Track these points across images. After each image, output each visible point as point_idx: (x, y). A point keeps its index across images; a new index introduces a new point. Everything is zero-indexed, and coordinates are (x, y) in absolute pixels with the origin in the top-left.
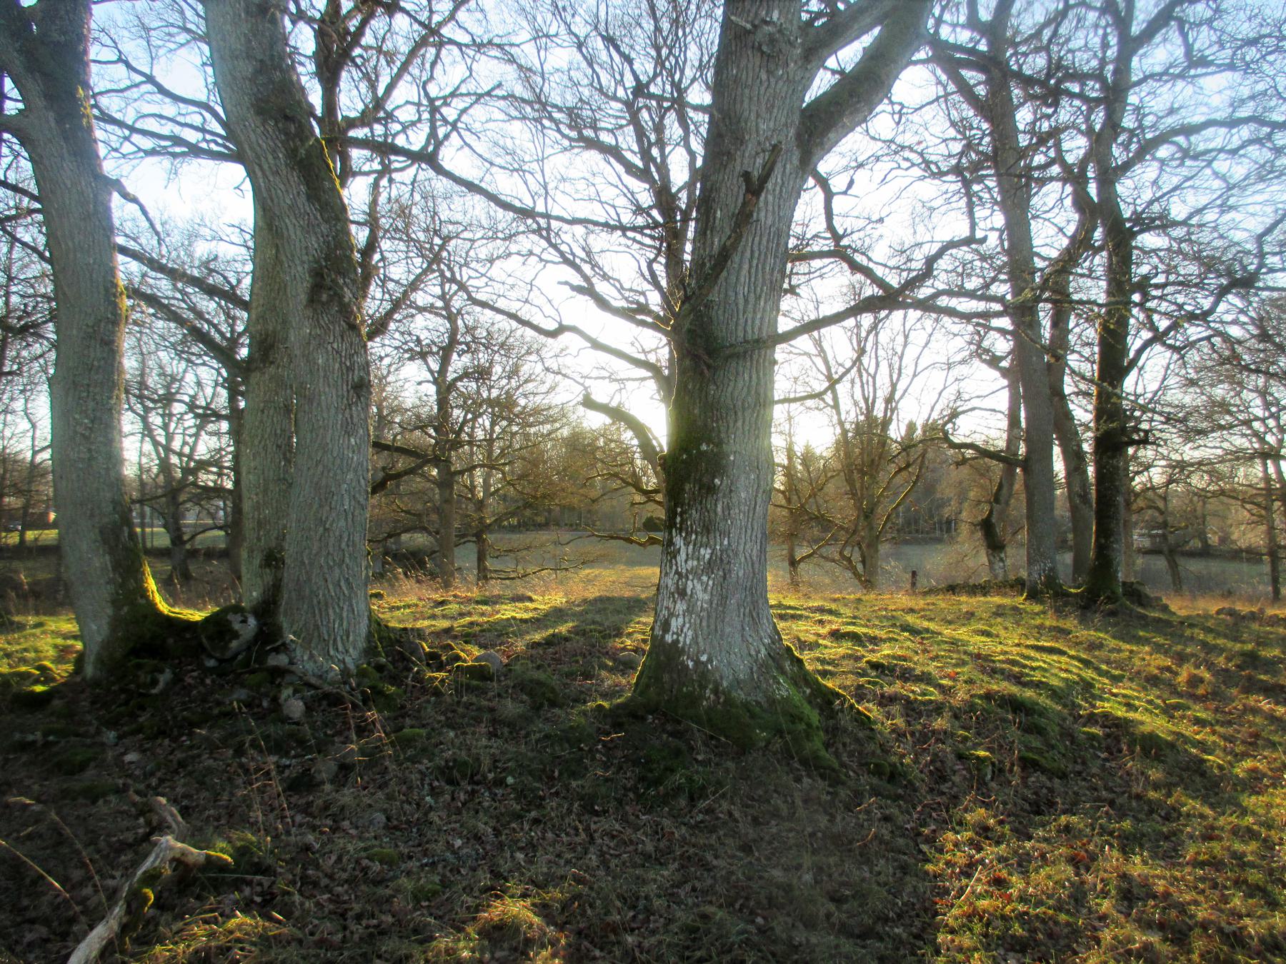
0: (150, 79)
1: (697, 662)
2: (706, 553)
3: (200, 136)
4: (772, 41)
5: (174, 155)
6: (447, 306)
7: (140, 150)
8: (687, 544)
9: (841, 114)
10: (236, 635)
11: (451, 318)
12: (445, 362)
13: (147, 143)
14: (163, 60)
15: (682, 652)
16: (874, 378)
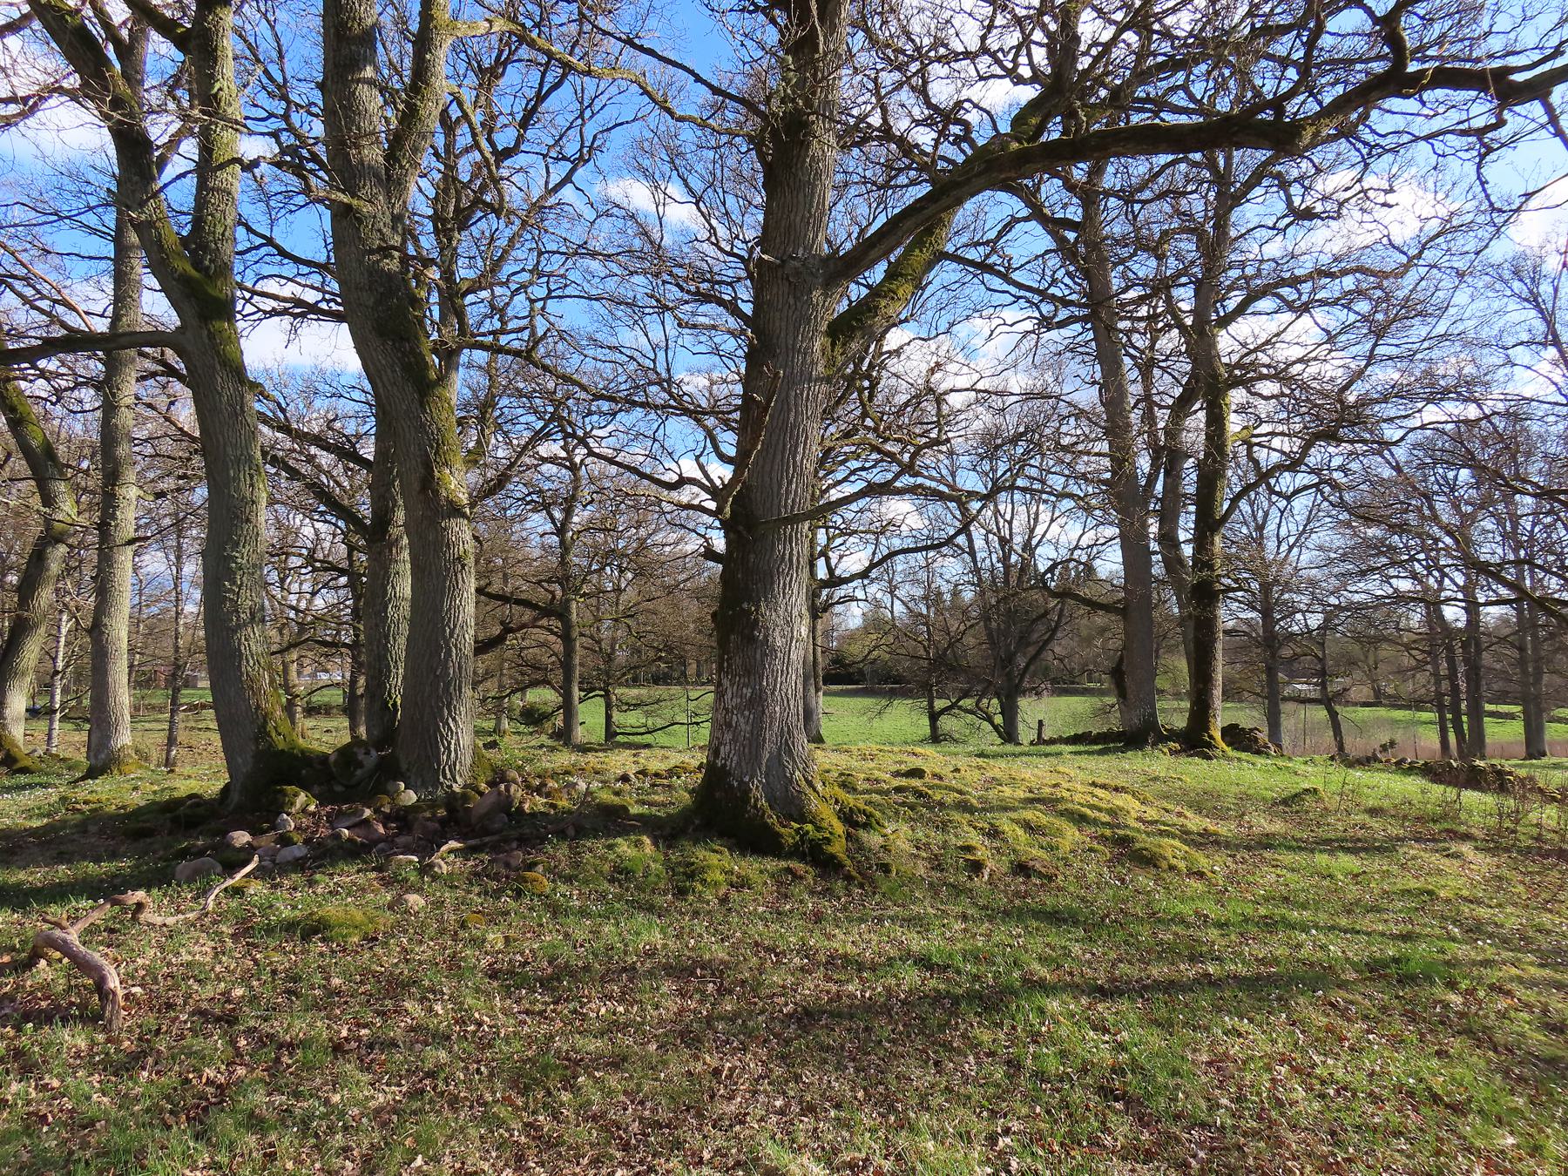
0: (270, 241)
1: (741, 782)
2: (748, 692)
3: (319, 296)
4: (797, 273)
5: (295, 316)
6: (570, 458)
7: (259, 310)
8: (732, 685)
9: (112, 817)
10: (360, 765)
11: (574, 468)
12: (568, 512)
13: (269, 304)
14: (282, 221)
15: (729, 774)
16: (1010, 523)
